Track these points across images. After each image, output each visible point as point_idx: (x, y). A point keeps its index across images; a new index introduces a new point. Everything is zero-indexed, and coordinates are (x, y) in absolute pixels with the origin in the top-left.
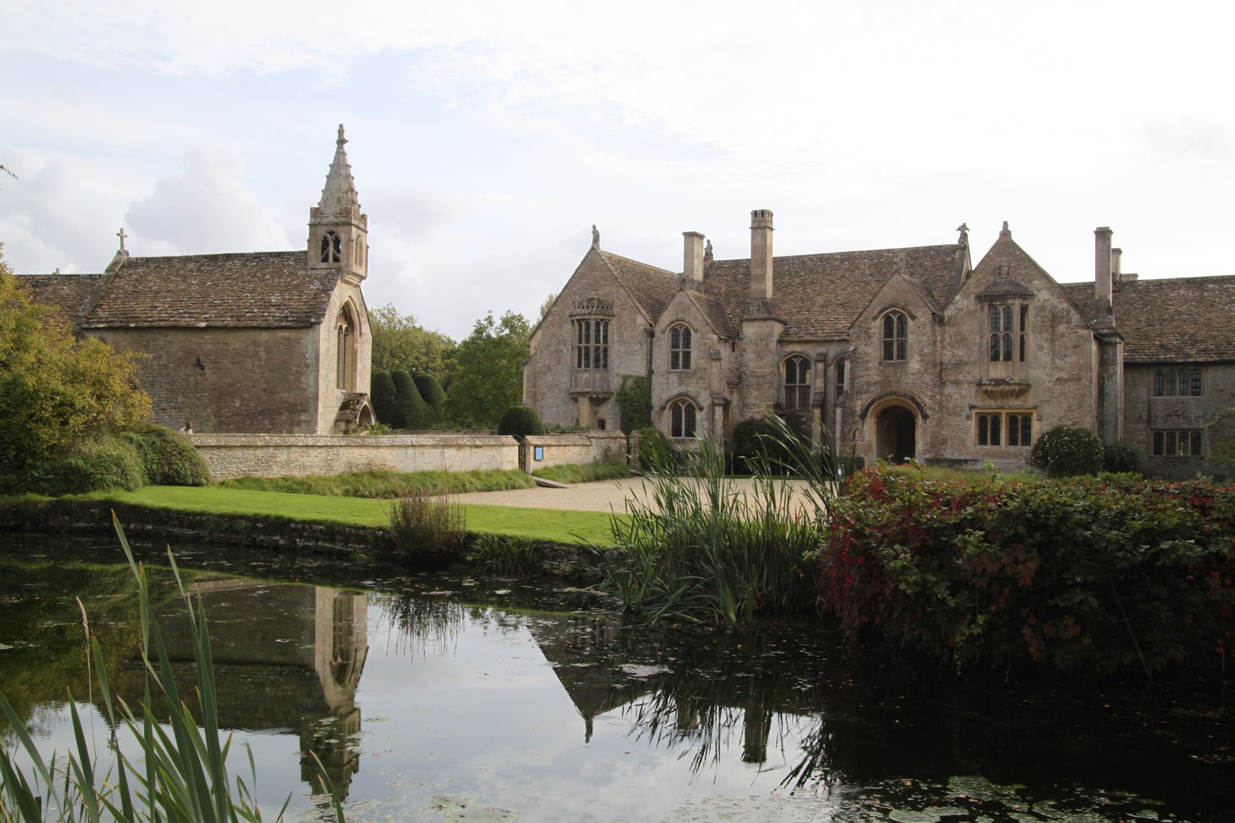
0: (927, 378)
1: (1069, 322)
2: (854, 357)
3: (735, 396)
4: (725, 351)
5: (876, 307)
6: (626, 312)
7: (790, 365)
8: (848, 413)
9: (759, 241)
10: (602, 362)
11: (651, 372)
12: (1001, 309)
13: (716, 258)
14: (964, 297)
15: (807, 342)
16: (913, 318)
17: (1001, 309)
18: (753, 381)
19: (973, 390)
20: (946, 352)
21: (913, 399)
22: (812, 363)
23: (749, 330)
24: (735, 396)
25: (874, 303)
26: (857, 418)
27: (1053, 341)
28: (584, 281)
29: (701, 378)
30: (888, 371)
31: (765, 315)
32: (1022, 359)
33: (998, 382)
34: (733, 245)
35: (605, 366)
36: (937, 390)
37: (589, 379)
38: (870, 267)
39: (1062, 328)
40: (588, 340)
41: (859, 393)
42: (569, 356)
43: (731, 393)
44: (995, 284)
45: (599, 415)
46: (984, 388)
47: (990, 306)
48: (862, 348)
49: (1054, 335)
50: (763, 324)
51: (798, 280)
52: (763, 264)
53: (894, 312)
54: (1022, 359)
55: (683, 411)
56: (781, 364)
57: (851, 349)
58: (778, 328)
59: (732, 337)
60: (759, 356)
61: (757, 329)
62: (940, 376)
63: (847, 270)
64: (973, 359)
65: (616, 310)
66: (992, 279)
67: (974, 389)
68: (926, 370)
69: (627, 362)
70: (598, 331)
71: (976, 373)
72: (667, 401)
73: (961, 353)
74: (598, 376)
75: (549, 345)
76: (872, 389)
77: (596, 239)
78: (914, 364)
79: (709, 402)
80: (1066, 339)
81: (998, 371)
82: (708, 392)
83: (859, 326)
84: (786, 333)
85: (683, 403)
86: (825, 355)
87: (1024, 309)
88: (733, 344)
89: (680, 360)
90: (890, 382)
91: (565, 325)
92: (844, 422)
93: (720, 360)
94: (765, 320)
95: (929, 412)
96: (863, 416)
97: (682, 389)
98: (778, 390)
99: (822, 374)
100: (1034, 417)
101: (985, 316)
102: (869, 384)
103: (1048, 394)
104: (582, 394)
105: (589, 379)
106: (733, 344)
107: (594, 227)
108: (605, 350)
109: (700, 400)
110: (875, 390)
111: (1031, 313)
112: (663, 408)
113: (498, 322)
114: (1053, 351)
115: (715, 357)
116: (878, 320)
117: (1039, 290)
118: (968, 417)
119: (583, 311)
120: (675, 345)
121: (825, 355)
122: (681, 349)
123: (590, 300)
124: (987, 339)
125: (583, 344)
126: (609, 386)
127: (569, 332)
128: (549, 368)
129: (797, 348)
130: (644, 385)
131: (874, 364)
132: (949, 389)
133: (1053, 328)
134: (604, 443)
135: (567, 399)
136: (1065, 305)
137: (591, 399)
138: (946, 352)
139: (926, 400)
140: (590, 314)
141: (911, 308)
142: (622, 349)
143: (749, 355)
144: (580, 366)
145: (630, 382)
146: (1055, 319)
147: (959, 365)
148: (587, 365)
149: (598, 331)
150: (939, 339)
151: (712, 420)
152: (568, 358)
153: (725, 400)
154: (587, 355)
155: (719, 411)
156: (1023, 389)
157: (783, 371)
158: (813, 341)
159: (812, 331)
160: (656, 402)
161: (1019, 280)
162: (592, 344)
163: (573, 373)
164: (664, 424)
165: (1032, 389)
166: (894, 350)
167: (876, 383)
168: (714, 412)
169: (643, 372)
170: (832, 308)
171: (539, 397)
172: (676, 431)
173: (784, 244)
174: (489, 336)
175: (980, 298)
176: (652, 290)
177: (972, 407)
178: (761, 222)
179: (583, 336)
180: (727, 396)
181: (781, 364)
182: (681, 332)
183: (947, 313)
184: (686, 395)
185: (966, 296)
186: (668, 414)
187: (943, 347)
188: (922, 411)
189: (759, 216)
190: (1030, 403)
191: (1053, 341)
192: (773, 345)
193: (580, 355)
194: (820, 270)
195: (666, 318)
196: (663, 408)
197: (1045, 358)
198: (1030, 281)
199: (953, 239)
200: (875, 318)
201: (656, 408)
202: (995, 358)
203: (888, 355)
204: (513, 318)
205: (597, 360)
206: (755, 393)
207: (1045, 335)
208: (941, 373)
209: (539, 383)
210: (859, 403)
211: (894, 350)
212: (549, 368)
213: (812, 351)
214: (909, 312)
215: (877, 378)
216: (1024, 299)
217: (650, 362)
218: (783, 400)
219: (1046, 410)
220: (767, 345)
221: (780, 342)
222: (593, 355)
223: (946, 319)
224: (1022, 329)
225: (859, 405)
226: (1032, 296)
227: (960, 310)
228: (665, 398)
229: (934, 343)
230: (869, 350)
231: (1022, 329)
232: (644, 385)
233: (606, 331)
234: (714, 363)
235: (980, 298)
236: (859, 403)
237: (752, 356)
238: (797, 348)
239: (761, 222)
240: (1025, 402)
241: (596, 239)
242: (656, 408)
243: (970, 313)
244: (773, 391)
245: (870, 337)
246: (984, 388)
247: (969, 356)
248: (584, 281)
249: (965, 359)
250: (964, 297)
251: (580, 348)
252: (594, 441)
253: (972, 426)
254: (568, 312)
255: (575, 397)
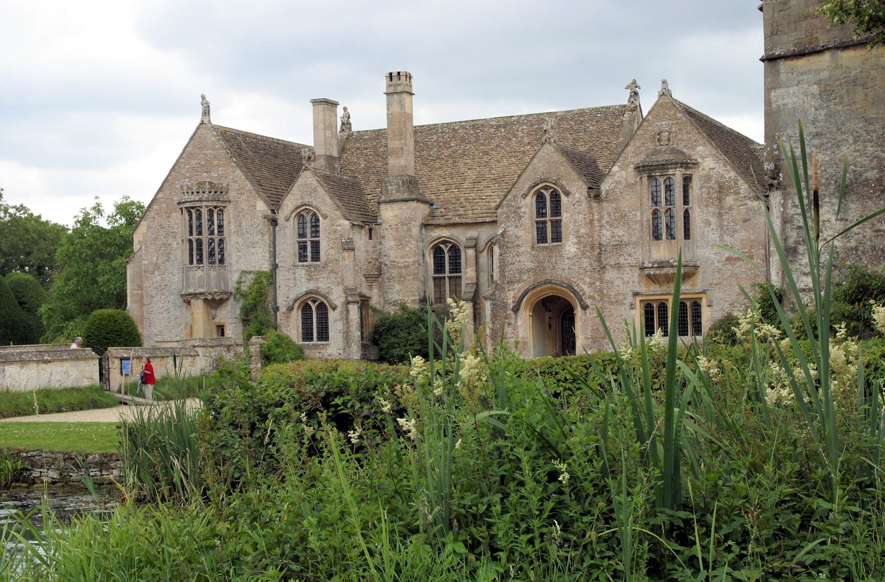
0: (585, 263)
1: (737, 193)
2: (501, 241)
3: (375, 291)
4: (360, 239)
5: (525, 183)
6: (244, 197)
7: (438, 252)
8: (499, 308)
9: (396, 109)
10: (217, 257)
11: (275, 267)
12: (661, 180)
13: (354, 129)
14: (622, 168)
15: (455, 225)
16: (567, 194)
17: (661, 180)
18: (395, 272)
19: (636, 274)
20: (604, 232)
21: (570, 287)
22: (462, 249)
23: (388, 213)
24: (375, 291)
25: (523, 177)
26: (510, 312)
27: (720, 215)
28: (194, 162)
29: (332, 271)
30: (542, 255)
31: (406, 196)
32: (687, 236)
33: (661, 265)
34: (369, 114)
35: (222, 261)
36: (597, 276)
37: (204, 278)
38: (529, 134)
39: (730, 200)
40: (200, 233)
41: (510, 282)
42: (180, 252)
43: (371, 287)
44: (655, 152)
45: (217, 320)
46: (646, 272)
47: (650, 177)
48: (512, 231)
49: (722, 208)
50: (404, 206)
51: (446, 152)
52: (401, 135)
53: (546, 188)
54: (687, 236)
55: (315, 315)
56: (427, 252)
57: (500, 231)
58: (422, 210)
59: (368, 222)
60: (401, 243)
61: (397, 212)
62: (599, 261)
63: (504, 138)
64: (634, 239)
65: (232, 195)
66: (651, 146)
67: (637, 272)
68: (584, 254)
69: (246, 256)
70: (211, 220)
71: (636, 255)
72: (295, 301)
73: (621, 233)
74: (213, 273)
75: (155, 239)
76: (525, 277)
77: (206, 112)
78: (570, 246)
79: (343, 300)
80: (735, 212)
81: (662, 251)
82: (341, 288)
83: (508, 206)
84: (432, 215)
85: (314, 301)
86: (476, 239)
87: (687, 180)
88: (370, 230)
89: (308, 251)
90: (544, 269)
91: (174, 214)
92: (494, 316)
93: (353, 250)
94: (406, 201)
95: (588, 302)
96: (516, 310)
97: (312, 286)
98: (424, 283)
99: (474, 263)
100: (704, 303)
101: (644, 187)
102: (521, 272)
103: (717, 276)
104: (195, 295)
105: (204, 278)
106: (370, 230)
107: (203, 98)
108: (221, 241)
109: (331, 297)
110: (528, 280)
111: (696, 185)
112: (291, 309)
113: (109, 209)
114: (721, 226)
115: (348, 247)
116: (529, 198)
117: (703, 158)
118: (632, 306)
119: (192, 198)
120: (540, 213)
121: (476, 239)
122: (309, 239)
123: (201, 184)
124: (648, 215)
125: (195, 237)
126: (227, 285)
127: (179, 222)
128: (157, 267)
129: (445, 233)
130: (267, 280)
131: (526, 248)
132: (610, 275)
133: (720, 200)
134: (214, 353)
135: (179, 301)
136: (733, 174)
137: (206, 300)
138: (604, 232)
139: (585, 288)
140: (200, 201)
141: (564, 183)
142: (240, 241)
143: (389, 244)
144: (191, 262)
145: (249, 280)
146: (722, 190)
147: (619, 246)
148: (200, 261)
149: (211, 220)
150: (596, 217)
151: (347, 320)
152: (178, 253)
153: (361, 296)
154: (200, 249)
155: (354, 310)
156: (689, 273)
157: (430, 260)
158: (462, 224)
159: (462, 211)
160: (282, 302)
161: (681, 147)
162: (205, 237)
163: (185, 271)
164: (292, 327)
165: (700, 270)
166: (549, 231)
167: (528, 271)
168: (348, 311)
169: (266, 267)
170: (485, 183)
171: (146, 301)
172: (307, 335)
173: (424, 114)
174: (100, 230)
175: (640, 169)
176: (270, 163)
177: (636, 294)
178: (399, 85)
179: (195, 228)
180: (365, 291)
181: (427, 252)
182: (308, 218)
183: (605, 187)
184: (317, 292)
185: (623, 168)
186: (297, 316)
187: (601, 226)
188: (581, 301)
189: (395, 79)
190: (699, 287)
191: (720, 215)
192: (415, 231)
193: (191, 250)
194: (473, 139)
195: (289, 203)
196: (291, 309)
197: (713, 235)
198: (693, 148)
199: (622, 98)
200: (525, 196)
201: (283, 309)
202: (657, 237)
203: (542, 238)
204: (132, 203)
205: (211, 254)
206: (397, 287)
207: (711, 209)
208: (599, 255)
209: (146, 284)
210: (512, 294)
211: (549, 231)
212: (157, 267)
213: (461, 236)
214: (562, 187)
215: (529, 265)
216: (687, 168)
217: (274, 255)
218: (431, 293)
219: (717, 294)
220: (409, 230)
221: (425, 226)
222: (206, 249)
223: (603, 194)
224: (686, 202)
225: (510, 297)
226: (696, 164)
227: (618, 183)
228: (292, 296)
229: (591, 221)
230: (520, 233)
231: (686, 202)
232: (267, 280)
233: (221, 220)
234: (346, 254)
235: (640, 169)
236: (512, 294)
237: (393, 243)
238: (445, 233)
239: (399, 85)
240: (693, 285)
241: (206, 112)
242: (283, 309)
243: (629, 186)
244: (417, 284)
245: (520, 217)
246: (646, 272)
247: (631, 236)
248: (194, 162)
249: (625, 239)
250: (622, 168)
251: (190, 241)
252: (200, 350)
253: (637, 317)
254: (176, 199)
255: (187, 299)
